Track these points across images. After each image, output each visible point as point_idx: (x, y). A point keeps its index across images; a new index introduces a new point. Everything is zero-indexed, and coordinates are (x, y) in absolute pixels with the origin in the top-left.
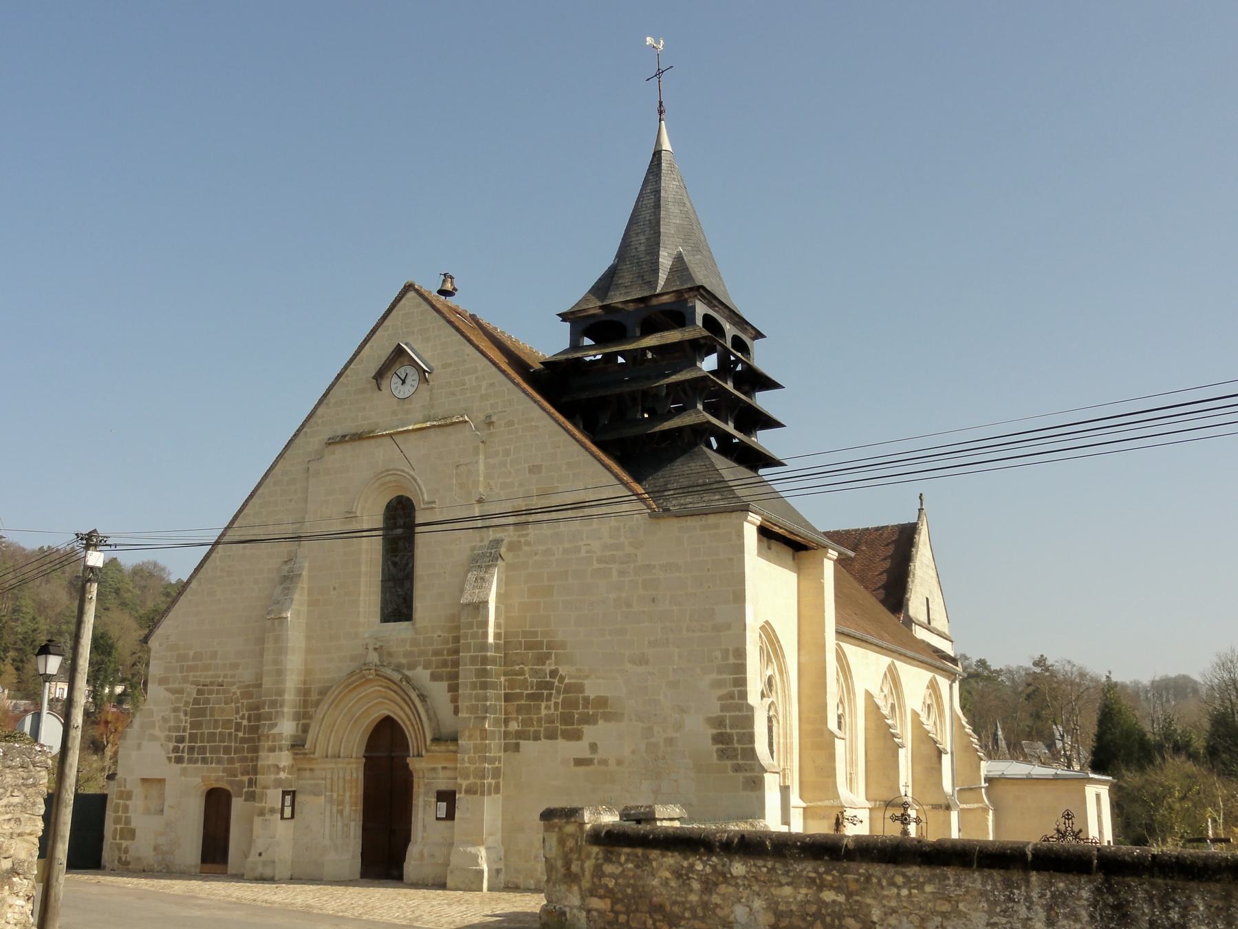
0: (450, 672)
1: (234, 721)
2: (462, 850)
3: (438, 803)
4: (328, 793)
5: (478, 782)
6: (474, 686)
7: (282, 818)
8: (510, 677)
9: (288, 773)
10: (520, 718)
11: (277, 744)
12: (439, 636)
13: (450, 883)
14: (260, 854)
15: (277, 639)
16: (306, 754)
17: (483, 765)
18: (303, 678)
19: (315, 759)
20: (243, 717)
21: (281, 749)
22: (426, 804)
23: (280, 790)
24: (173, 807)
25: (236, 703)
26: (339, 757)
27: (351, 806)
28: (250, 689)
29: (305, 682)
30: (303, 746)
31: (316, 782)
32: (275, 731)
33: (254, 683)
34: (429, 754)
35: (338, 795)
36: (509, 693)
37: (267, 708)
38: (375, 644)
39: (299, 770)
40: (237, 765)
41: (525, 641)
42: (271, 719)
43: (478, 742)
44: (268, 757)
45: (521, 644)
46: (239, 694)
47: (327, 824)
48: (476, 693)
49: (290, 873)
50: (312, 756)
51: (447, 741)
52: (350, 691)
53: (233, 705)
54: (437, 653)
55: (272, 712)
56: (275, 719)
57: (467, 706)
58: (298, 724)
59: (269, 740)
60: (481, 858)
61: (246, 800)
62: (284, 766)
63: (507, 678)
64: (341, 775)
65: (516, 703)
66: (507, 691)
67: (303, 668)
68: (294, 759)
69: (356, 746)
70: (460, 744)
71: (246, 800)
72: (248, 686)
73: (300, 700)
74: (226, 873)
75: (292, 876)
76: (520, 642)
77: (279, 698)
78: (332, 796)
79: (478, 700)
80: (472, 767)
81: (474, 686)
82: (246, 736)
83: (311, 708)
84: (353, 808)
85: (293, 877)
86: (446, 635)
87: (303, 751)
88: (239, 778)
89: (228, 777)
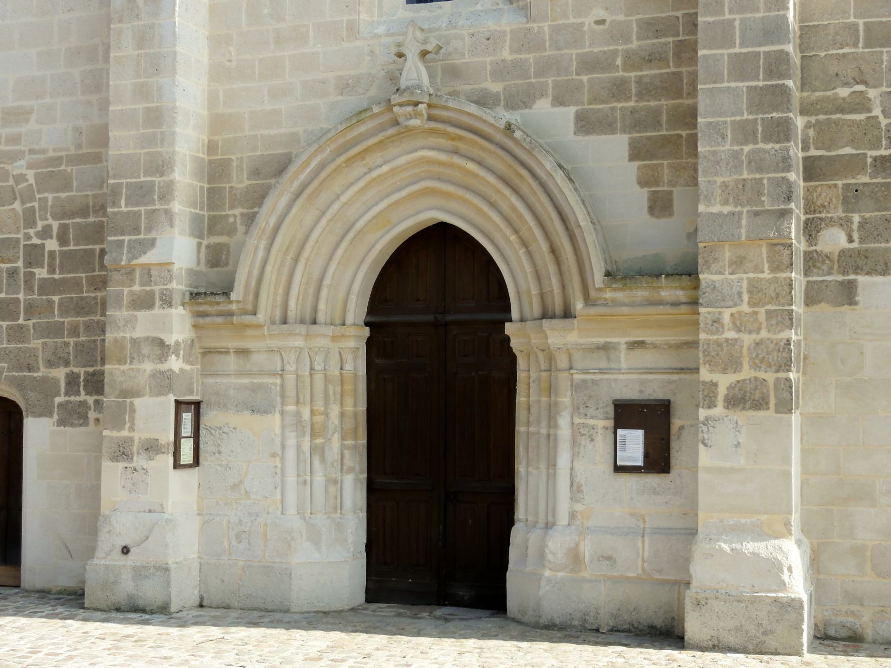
0: (633, 111)
1: (22, 243)
2: (725, 547)
3: (620, 432)
4: (291, 408)
5: (770, 377)
6: (746, 132)
7: (177, 465)
8: (822, 117)
9: (187, 360)
10: (856, 218)
11: (157, 288)
12: (601, 22)
13: (692, 627)
14: (126, 550)
15: (143, 39)
16: (231, 314)
17: (785, 335)
18: (205, 138)
19: (259, 326)
20: (45, 233)
21: (168, 302)
22: (577, 433)
23: (172, 398)
24: (607, 429)
25: (23, 202)
26: (314, 322)
27: (343, 439)
28: (63, 167)
29: (212, 147)
30: (226, 294)
31: (257, 380)
32: (150, 257)
33: (72, 151)
34: (592, 311)
35: (312, 412)
36: (820, 157)
37: (123, 203)
38: (425, 42)
39: (207, 352)
40: (36, 343)
41: (865, 23)
42: (136, 230)
43: (767, 275)
44: (131, 322)
45: (858, 31)
46: (32, 180)
47: (291, 479)
48: (753, 152)
49: (196, 592)
50: (248, 319)
51: (658, 276)
52: (349, 162)
53: (17, 205)
54: (589, 64)
55: (138, 215)
56: (149, 229)
57: (725, 185)
58: (199, 245)
59: (133, 280)
60: (790, 569)
61: (62, 423)
62: (177, 343)
63: (813, 119)
64: (318, 367)
65: (840, 183)
66: (813, 152)
67: (205, 112)
68: (195, 326)
69: (353, 298)
70: (703, 284)
71: (62, 423)
72: (58, 160)
73: (202, 188)
74: (18, 586)
75: (202, 598)
76: (854, 27)
77: (157, 179)
78: (298, 414)
79: (760, 169)
80: (748, 340)
81: (746, 132)
82: (57, 276)
83: (232, 207)
84: (349, 442)
85: (204, 603)
86: (621, 17)
87: (223, 307)
88: (42, 372)
89: (9, 371)
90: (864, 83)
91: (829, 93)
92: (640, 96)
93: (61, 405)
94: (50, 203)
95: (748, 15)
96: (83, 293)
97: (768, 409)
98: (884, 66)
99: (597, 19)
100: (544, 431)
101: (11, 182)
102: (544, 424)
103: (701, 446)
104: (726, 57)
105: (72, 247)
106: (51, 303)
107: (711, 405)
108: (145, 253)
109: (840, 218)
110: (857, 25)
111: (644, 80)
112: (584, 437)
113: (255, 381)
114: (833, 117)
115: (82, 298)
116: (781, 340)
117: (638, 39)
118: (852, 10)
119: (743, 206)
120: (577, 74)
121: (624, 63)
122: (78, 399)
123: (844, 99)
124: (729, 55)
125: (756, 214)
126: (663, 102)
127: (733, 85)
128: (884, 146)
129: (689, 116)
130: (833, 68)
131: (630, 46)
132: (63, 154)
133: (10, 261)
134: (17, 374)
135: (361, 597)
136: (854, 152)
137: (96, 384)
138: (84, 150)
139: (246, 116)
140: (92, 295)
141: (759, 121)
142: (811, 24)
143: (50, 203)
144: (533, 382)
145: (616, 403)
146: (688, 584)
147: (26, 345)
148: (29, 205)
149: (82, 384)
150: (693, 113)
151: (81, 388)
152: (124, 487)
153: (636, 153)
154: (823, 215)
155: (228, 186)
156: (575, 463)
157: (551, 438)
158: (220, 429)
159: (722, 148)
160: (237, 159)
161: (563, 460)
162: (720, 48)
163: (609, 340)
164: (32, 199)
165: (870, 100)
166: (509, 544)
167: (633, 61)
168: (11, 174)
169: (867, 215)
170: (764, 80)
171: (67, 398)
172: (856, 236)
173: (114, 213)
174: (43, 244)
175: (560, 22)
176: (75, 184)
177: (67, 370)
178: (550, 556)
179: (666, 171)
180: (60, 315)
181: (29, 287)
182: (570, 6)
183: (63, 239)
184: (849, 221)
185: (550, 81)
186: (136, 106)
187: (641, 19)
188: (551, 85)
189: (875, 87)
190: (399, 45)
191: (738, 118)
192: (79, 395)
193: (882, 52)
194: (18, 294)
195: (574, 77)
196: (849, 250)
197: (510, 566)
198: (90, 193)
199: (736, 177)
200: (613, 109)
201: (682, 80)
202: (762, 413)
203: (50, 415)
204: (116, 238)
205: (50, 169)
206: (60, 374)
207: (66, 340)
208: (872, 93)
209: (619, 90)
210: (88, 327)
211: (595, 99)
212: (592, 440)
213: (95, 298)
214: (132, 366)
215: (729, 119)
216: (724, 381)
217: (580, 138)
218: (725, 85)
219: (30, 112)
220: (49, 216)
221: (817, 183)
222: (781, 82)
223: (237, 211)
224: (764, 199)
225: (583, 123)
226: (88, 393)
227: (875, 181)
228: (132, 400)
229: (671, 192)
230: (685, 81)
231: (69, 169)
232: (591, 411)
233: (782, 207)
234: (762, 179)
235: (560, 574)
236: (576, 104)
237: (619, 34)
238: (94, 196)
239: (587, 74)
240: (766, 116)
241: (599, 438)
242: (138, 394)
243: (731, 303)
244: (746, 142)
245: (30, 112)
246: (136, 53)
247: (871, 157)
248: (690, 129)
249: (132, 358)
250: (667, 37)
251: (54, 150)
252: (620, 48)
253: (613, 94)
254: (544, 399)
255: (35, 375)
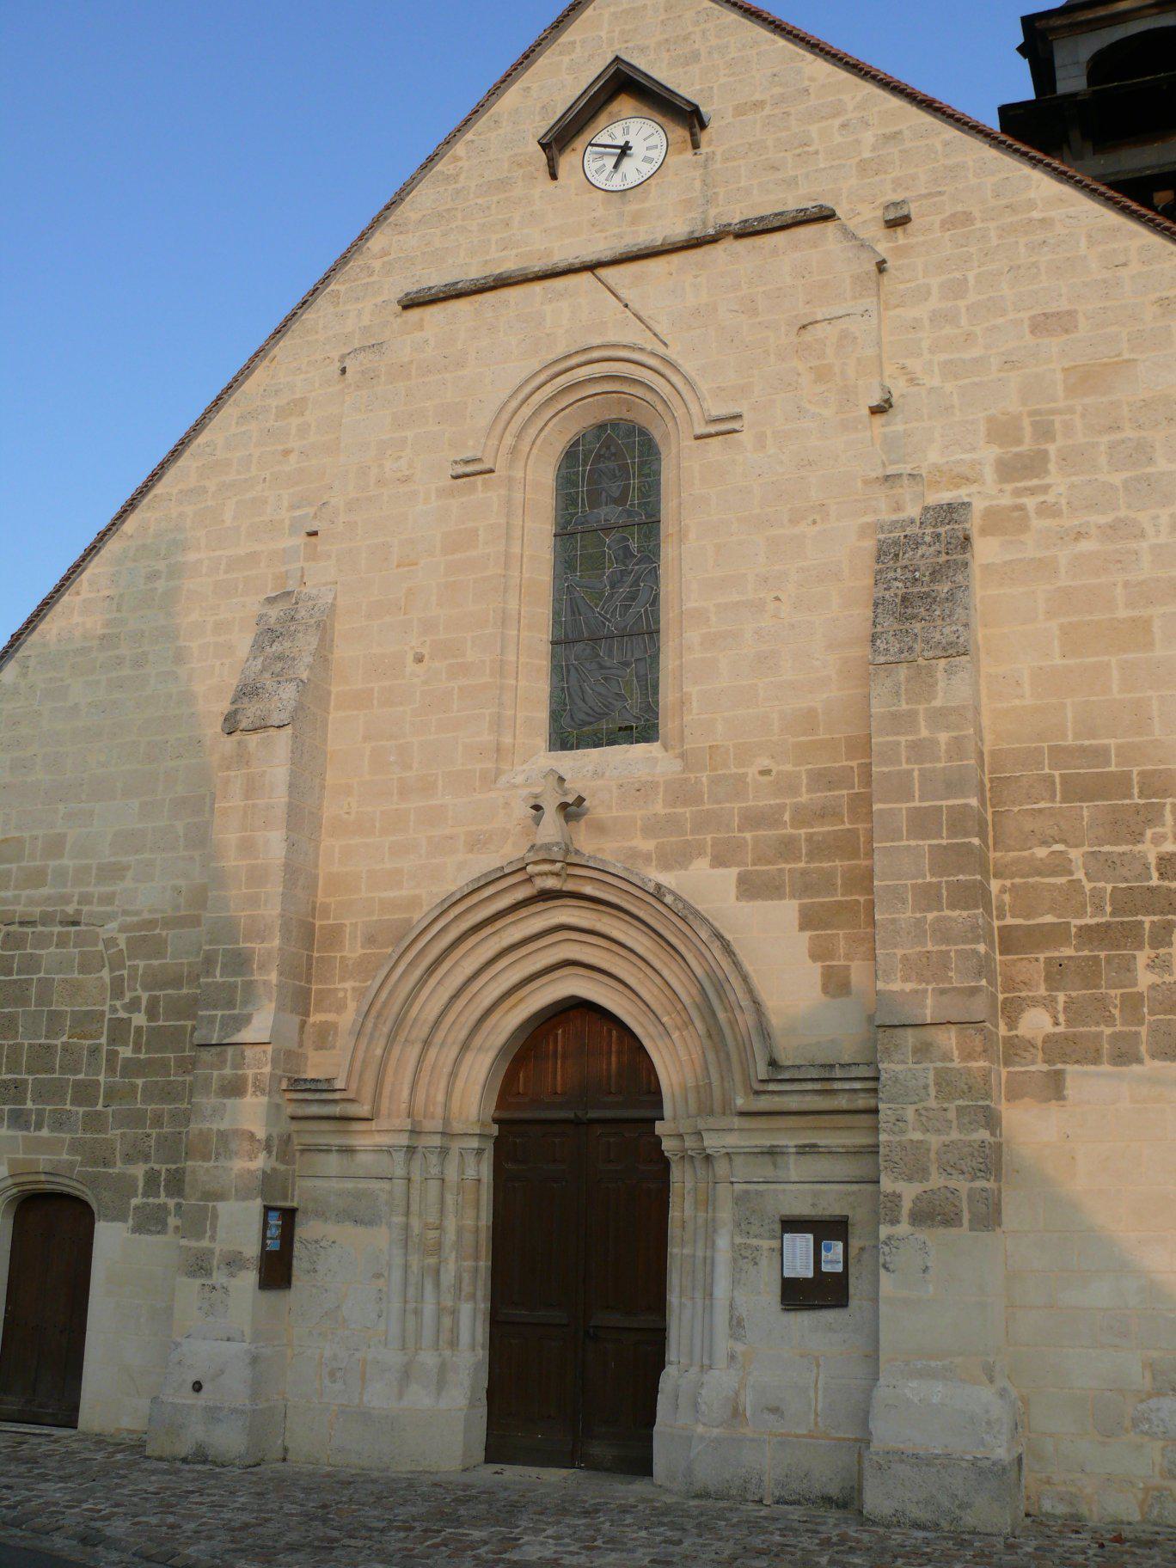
0: (804, 872)
1: (108, 1016)
6: (928, 897)
8: (1017, 880)
10: (1061, 997)
12: (765, 772)
20: (134, 1006)
25: (112, 970)
28: (157, 931)
40: (114, 1133)
42: (231, 1004)
45: (1053, 783)
46: (123, 946)
48: (938, 920)
53: (105, 974)
54: (753, 820)
55: (233, 986)
56: (245, 1003)
57: (905, 957)
63: (1008, 883)
65: (1042, 957)
71: (137, 1229)
72: (152, 924)
76: (1049, 780)
80: (934, 1141)
81: (928, 897)
82: (142, 1056)
83: (342, 979)
86: (788, 767)
88: (118, 1168)
89: (82, 1165)
90: (1064, 841)
91: (1026, 853)
92: (811, 856)
93: (138, 1207)
94: (140, 972)
95: (927, 765)
96: (169, 1076)
97: (961, 1226)
98: (1085, 823)
99: (761, 769)
100: (700, 1253)
101: (101, 947)
102: (700, 1244)
103: (882, 1271)
104: (904, 812)
105: (161, 1023)
106: (134, 1086)
107: (895, 1221)
108: (239, 1031)
109: (1045, 998)
110: (1053, 776)
111: (815, 838)
112: (746, 1260)
113: (360, 1186)
114: (1031, 880)
115: (170, 1083)
116: (975, 1141)
117: (809, 791)
118: (1046, 761)
119: (928, 983)
120: (739, 831)
121: (793, 818)
122: (157, 1201)
123: (1041, 860)
124: (908, 809)
125: (943, 992)
126: (837, 863)
127: (913, 843)
128: (1089, 914)
129: (863, 880)
130: (1028, 825)
131: (799, 799)
132: (158, 916)
133: (92, 1037)
134: (90, 1170)
135: (480, 1454)
136: (1056, 920)
137: (176, 1184)
138: (183, 913)
139: (364, 876)
140: (180, 1079)
141: (944, 885)
142: (1002, 775)
143: (140, 972)
144: (689, 1192)
145: (783, 1219)
146: (868, 1443)
147: (104, 1136)
148: (117, 973)
149: (163, 1183)
150: (869, 875)
151: (162, 1188)
152: (200, 1308)
153: (808, 921)
154: (1023, 994)
155: (339, 955)
156: (736, 1293)
157: (708, 1261)
158: (316, 1242)
159: (903, 916)
160: (351, 924)
161: (722, 1289)
162: (896, 801)
163: (775, 1143)
164: (122, 966)
165: (1071, 861)
166: (657, 1392)
167: (802, 816)
168: (101, 937)
169: (1074, 994)
170: (948, 838)
171: (145, 1200)
172: (1061, 1018)
173: (207, 984)
174: (130, 1019)
175: (720, 772)
176: (169, 950)
177: (147, 1167)
178: (703, 1407)
179: (842, 943)
180: (143, 1102)
181: (111, 1069)
182: (732, 755)
183: (152, 1014)
184: (1054, 1000)
185: (709, 838)
186: (240, 863)
187: (811, 770)
188: (710, 843)
189: (1076, 846)
190: (536, 796)
191: (920, 881)
192: (159, 1197)
193: (1082, 808)
194: (98, 1075)
195: (737, 834)
196: (1054, 1034)
197: (658, 1420)
198: (185, 961)
199: (919, 949)
200: (781, 870)
201: (858, 838)
202: (953, 1231)
203: (125, 1220)
204: (208, 1013)
205: (143, 933)
206: (139, 1171)
207: (148, 1131)
208: (1075, 854)
209: (787, 848)
210: (174, 1115)
211: (759, 859)
212: (756, 1264)
213: (184, 1082)
214: (216, 1164)
215: (909, 882)
216: (909, 1192)
217: (743, 903)
218: (905, 843)
219: (127, 868)
220: (138, 986)
221: (1016, 957)
222: (967, 840)
223: (349, 985)
224: (951, 974)
225: (746, 886)
226: (169, 1194)
227: (1080, 954)
228: (215, 1203)
229: (848, 968)
230: (862, 839)
231: (164, 933)
232: (754, 1229)
233: (972, 984)
234: (948, 952)
235: (716, 1431)
236: (738, 865)
237: (787, 786)
238: (190, 965)
239: (751, 831)
240: (952, 878)
241: (764, 1262)
242: (220, 1196)
243: (916, 1098)
244: (929, 909)
245: (127, 868)
246: (242, 804)
247: (1075, 926)
248: (868, 895)
249: (218, 1154)
250: (841, 789)
251: (150, 911)
252: (788, 801)
253: (780, 853)
254: (701, 1214)
255: (111, 1171)
